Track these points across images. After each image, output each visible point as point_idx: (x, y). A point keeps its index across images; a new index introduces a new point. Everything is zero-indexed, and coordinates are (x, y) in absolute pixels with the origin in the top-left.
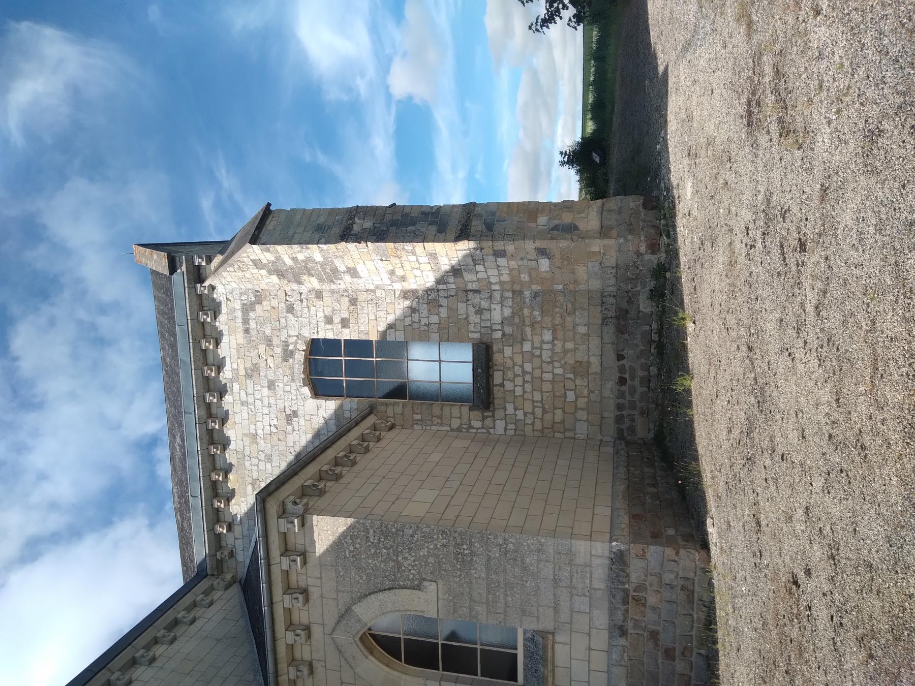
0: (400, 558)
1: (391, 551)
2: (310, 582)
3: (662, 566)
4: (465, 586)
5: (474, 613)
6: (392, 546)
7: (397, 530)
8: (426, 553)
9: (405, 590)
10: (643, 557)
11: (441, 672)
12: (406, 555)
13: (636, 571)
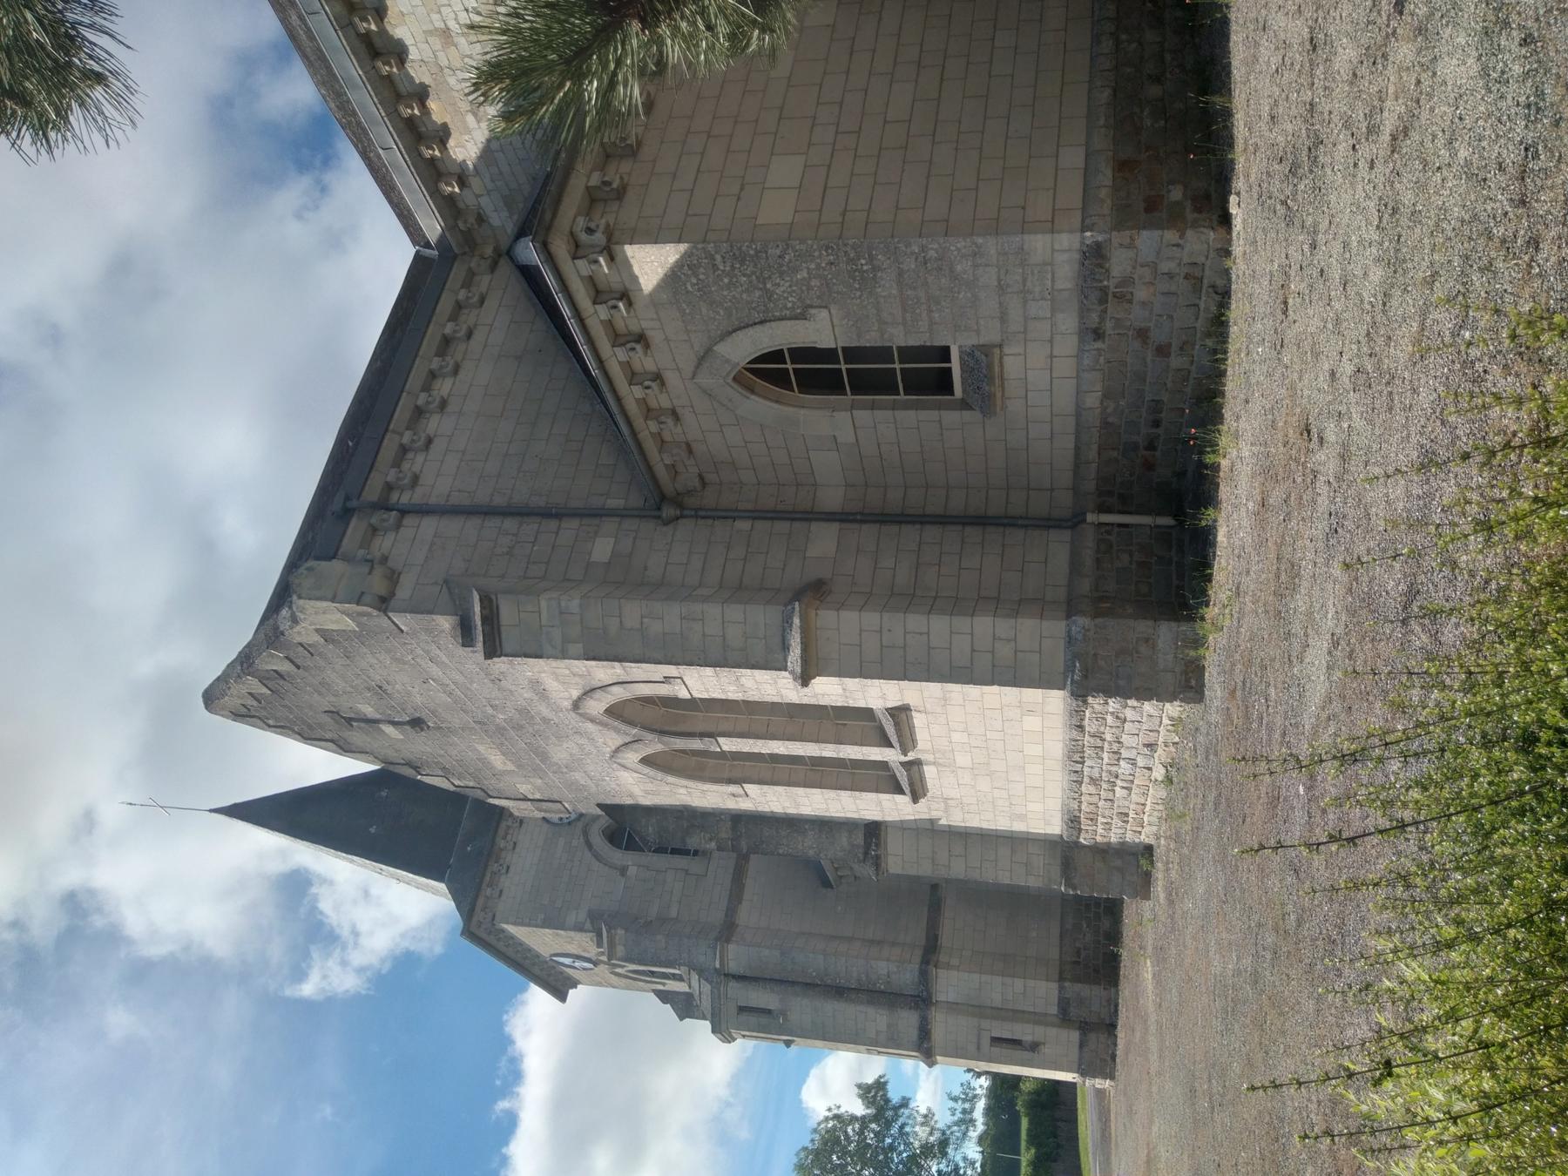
0: (769, 286)
1: (754, 277)
2: (644, 324)
3: (1158, 253)
4: (869, 307)
5: (886, 336)
6: (753, 273)
7: (757, 252)
8: (806, 275)
9: (784, 322)
10: (1131, 246)
11: (850, 397)
12: (778, 281)
13: (1119, 263)
